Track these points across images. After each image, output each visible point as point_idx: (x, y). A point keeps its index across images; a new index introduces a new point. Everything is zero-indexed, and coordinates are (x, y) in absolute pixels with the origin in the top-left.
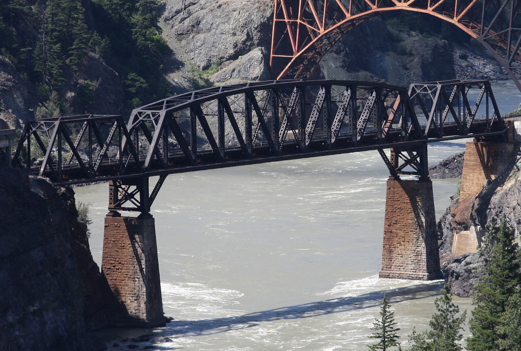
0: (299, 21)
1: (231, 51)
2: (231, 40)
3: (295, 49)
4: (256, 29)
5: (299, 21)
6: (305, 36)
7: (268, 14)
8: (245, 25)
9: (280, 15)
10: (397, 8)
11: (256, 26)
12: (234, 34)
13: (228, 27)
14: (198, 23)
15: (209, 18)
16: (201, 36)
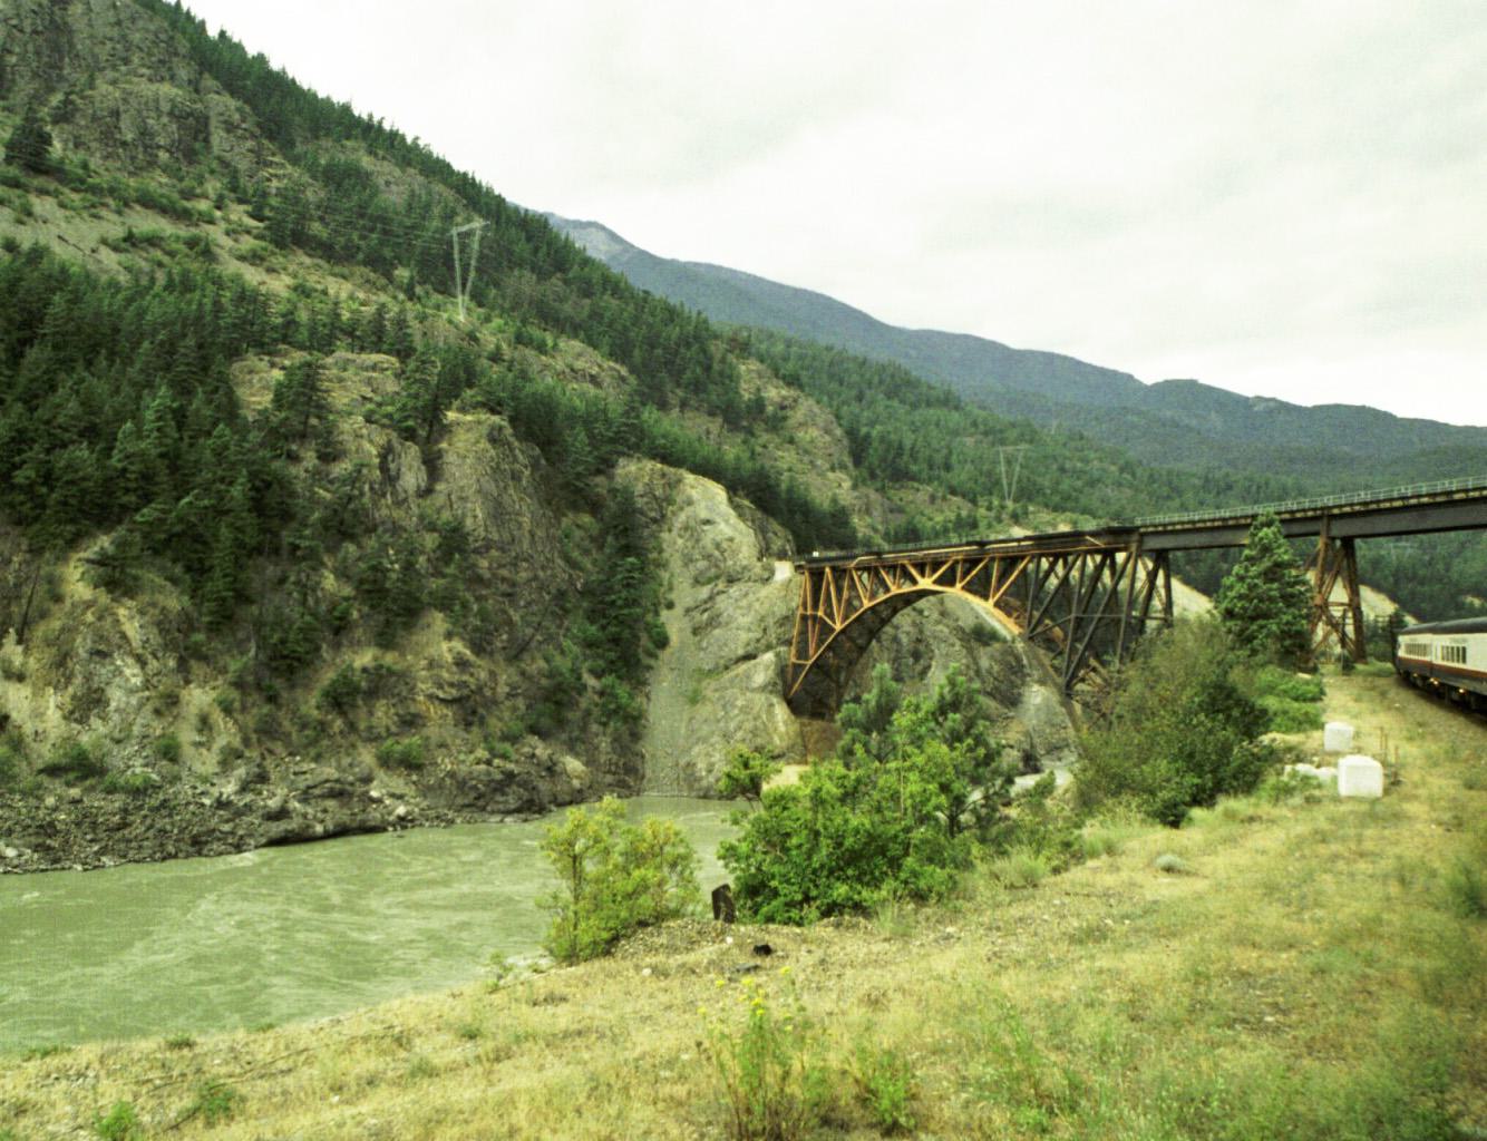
1: (741, 652)
2: (744, 636)
3: (811, 652)
7: (794, 605)
8: (762, 619)
9: (805, 605)
12: (749, 630)
13: (744, 621)
14: (718, 616)
15: (731, 610)
16: (717, 632)
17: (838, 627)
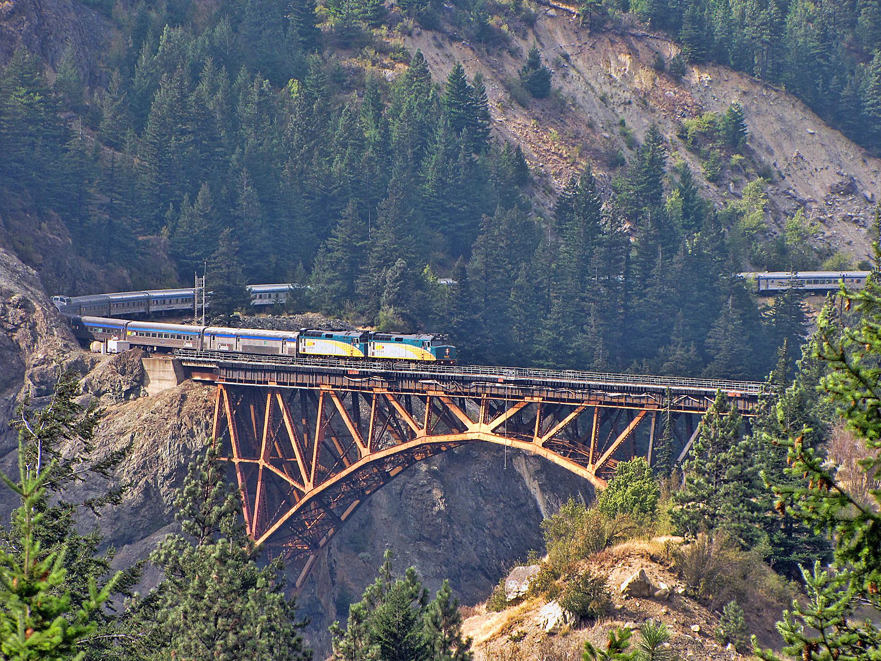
0: (261, 462)
4: (166, 478)
5: (261, 462)
6: (278, 495)
10: (468, 436)
11: (167, 471)
17: (310, 490)
